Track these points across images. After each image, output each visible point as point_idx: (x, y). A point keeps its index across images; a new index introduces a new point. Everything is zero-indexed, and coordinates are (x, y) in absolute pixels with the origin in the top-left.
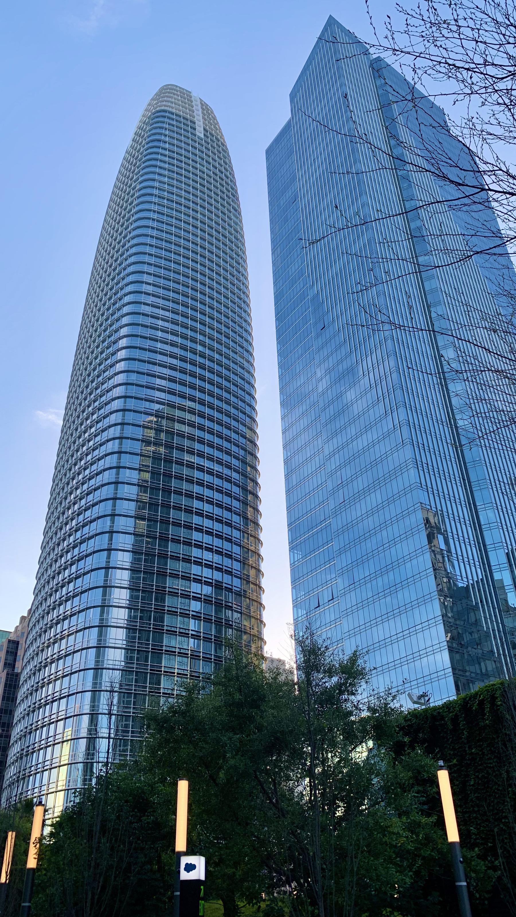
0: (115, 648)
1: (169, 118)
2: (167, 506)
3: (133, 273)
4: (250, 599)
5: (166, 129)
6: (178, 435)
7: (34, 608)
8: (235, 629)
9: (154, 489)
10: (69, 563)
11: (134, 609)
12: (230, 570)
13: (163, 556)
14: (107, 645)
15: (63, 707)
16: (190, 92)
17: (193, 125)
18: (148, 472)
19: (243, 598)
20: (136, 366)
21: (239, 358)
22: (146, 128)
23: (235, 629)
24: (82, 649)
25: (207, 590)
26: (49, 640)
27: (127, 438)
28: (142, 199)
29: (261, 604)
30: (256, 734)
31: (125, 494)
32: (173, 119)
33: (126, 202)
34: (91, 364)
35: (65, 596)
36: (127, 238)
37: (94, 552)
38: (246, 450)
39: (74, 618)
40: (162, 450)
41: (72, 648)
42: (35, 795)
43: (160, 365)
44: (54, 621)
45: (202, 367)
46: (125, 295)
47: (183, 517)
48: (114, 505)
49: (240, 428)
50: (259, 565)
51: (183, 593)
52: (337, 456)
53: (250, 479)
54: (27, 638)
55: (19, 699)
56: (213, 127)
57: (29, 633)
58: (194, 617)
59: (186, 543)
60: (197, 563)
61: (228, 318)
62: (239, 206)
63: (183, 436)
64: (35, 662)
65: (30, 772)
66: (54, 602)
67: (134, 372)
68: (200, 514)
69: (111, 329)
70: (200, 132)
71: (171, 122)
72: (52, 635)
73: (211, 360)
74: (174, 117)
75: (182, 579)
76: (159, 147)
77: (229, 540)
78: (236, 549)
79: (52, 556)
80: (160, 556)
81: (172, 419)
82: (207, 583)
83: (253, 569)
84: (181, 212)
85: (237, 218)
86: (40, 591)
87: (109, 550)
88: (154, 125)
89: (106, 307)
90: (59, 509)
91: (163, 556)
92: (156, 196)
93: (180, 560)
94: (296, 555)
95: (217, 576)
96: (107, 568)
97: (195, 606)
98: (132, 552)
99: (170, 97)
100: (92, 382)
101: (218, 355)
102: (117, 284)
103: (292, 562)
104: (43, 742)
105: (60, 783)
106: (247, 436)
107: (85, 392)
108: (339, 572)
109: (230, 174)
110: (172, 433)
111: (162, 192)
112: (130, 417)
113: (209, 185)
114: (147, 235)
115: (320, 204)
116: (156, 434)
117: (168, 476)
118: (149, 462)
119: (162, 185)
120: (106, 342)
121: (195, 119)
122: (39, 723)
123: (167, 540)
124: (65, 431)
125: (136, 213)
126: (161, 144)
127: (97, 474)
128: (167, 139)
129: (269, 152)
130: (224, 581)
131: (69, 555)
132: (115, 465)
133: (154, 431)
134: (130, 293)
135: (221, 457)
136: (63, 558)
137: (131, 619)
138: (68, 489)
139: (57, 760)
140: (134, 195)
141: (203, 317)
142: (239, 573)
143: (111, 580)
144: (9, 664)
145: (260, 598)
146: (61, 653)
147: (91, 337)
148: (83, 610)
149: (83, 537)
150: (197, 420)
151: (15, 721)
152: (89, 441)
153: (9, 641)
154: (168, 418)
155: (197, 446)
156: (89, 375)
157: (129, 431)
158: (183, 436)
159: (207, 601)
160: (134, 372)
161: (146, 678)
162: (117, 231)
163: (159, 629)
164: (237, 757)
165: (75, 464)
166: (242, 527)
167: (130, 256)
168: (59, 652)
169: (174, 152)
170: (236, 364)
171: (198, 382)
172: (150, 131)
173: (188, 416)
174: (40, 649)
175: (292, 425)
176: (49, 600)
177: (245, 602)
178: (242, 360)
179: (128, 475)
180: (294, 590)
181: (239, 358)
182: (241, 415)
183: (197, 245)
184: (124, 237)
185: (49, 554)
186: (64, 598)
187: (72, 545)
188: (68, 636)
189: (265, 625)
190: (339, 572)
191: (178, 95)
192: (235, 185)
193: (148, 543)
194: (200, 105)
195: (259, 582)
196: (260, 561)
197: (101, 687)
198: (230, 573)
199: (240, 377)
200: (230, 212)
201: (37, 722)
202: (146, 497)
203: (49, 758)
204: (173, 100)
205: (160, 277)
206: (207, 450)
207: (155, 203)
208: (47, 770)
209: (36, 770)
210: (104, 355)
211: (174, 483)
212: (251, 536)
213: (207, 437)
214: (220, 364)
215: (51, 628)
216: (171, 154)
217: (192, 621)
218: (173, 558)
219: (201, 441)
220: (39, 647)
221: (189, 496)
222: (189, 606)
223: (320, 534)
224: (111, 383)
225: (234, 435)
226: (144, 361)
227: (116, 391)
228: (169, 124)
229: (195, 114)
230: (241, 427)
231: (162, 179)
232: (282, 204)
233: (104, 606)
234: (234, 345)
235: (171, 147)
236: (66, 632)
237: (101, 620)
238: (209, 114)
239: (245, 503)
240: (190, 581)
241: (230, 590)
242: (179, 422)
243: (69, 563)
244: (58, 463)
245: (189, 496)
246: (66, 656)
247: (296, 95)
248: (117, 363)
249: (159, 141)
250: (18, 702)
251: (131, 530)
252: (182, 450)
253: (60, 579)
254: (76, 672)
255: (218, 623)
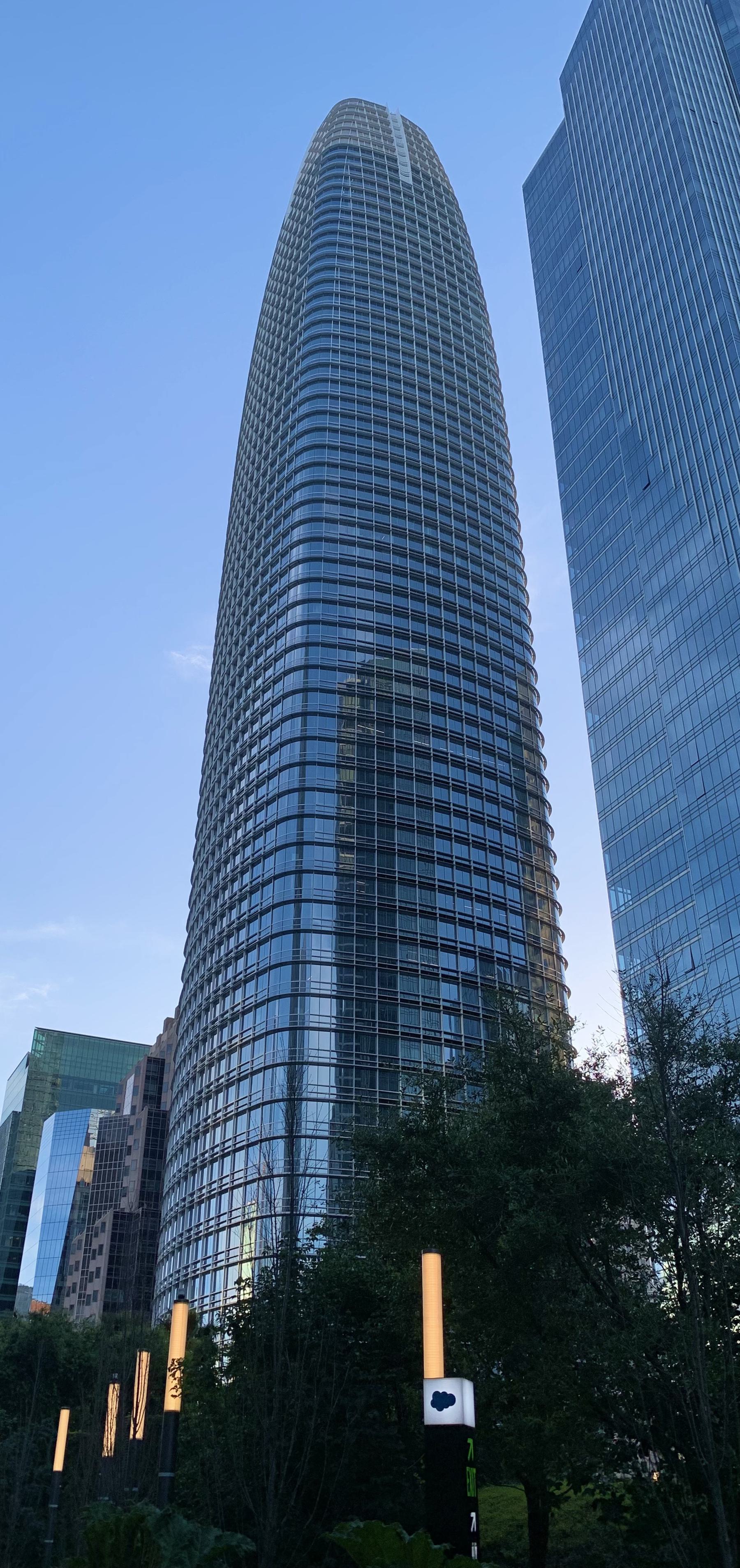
0: (318, 1064)
1: (351, 158)
2: (387, 825)
3: (306, 449)
4: (542, 978)
5: (346, 178)
6: (399, 702)
7: (184, 1003)
8: (516, 969)
9: (365, 797)
10: (235, 925)
11: (346, 999)
12: (505, 929)
13: (388, 910)
14: (306, 1025)
15: (240, 1164)
16: (384, 108)
17: (392, 165)
18: (352, 768)
19: (530, 977)
20: (322, 590)
21: (496, 562)
22: (313, 181)
23: (516, 969)
24: (265, 1068)
25: (467, 965)
26: (211, 1054)
27: (314, 738)
28: (314, 303)
29: (563, 986)
30: (564, 1167)
31: (317, 835)
32: (358, 159)
33: (290, 299)
34: (247, 594)
35: (230, 1012)
36: (293, 389)
37: (274, 906)
38: (518, 721)
39: (249, 1017)
40: (374, 730)
41: (249, 1066)
42: (205, 1308)
43: (361, 606)
44: (217, 1023)
45: (433, 582)
46: (296, 472)
47: (416, 841)
48: (300, 827)
49: (506, 683)
50: (555, 920)
51: (427, 969)
52: (686, 713)
53: (530, 771)
54: (176, 1052)
55: (170, 1153)
56: (427, 163)
57: (178, 1045)
58: (448, 1010)
59: (427, 975)
60: (446, 919)
61: (476, 510)
62: (482, 296)
63: (407, 704)
64: (191, 1092)
65: (194, 1272)
66: (215, 992)
67: (317, 601)
68: (444, 809)
69: (277, 531)
70: (406, 176)
71: (355, 164)
72: (215, 1046)
73: (449, 568)
74: (360, 154)
75: (423, 977)
76: (337, 211)
77: (500, 879)
78: (513, 894)
79: (204, 943)
80: (381, 823)
81: (385, 675)
82: (466, 953)
83: (544, 927)
84: (382, 318)
85: (480, 317)
86: (192, 974)
87: (297, 932)
88: (327, 174)
89: (265, 513)
90: (213, 839)
91: (388, 910)
92: (337, 295)
93: (416, 915)
94: (620, 895)
95: (483, 940)
96: (297, 932)
97: (449, 992)
98: (336, 903)
99: (350, 121)
100: (252, 624)
101: (459, 559)
102: (280, 472)
103: (615, 907)
104: (212, 1223)
105: (247, 1249)
106: (520, 696)
107: (240, 643)
108: (697, 886)
109: (463, 241)
110: (389, 700)
111: (346, 288)
112: (317, 678)
113: (427, 266)
114: (326, 365)
115: (627, 265)
116: (362, 705)
117: (386, 773)
118: (352, 752)
119: (346, 275)
120: (270, 555)
121: (396, 154)
122: (204, 1191)
123: (391, 881)
124: (213, 710)
125: (306, 328)
126: (341, 205)
127: (270, 777)
128: (350, 195)
129: (528, 188)
130: (495, 949)
131: (234, 914)
132: (296, 785)
133: (357, 700)
134: (304, 467)
135: (476, 736)
136: (227, 892)
137: (342, 1018)
138: (222, 830)
139: (237, 1252)
140: (299, 298)
141: (430, 496)
142: (521, 934)
143: (304, 952)
144: (152, 1098)
145: (561, 976)
146: (231, 1075)
147: (245, 549)
148: (262, 1004)
149: (253, 911)
150: (430, 674)
151: (166, 1190)
152: (251, 746)
153: (150, 1060)
154: (380, 675)
155: (432, 720)
156: (244, 634)
157: (317, 701)
158: (407, 704)
159: (467, 982)
160: (317, 601)
161: (374, 1041)
162: (275, 365)
163: (390, 999)
164: (531, 1211)
165: (234, 764)
166: (515, 803)
167: (300, 420)
168: (228, 1074)
169: (362, 216)
170: (494, 590)
171: (427, 609)
172: (319, 184)
173: (413, 669)
174: (198, 1069)
175: (600, 665)
176: (204, 1018)
177: (534, 984)
178: (502, 565)
179: (317, 802)
180: (607, 856)
181: (496, 562)
182: (506, 661)
183: (411, 342)
184: (288, 389)
185: (202, 913)
186: (230, 984)
187: (237, 897)
188: (241, 1046)
189: (566, 964)
190: (697, 886)
191: (363, 116)
192: (473, 259)
193: (360, 887)
194: (402, 128)
195: (558, 948)
196: (557, 912)
197: (304, 1023)
198: (504, 934)
199: (501, 595)
200: (467, 308)
201: (200, 1190)
202: (353, 811)
203: (226, 1210)
204: (356, 126)
205: (353, 469)
206: (450, 725)
207: (336, 308)
208: (221, 1268)
209: (204, 1268)
210: (266, 597)
211: (398, 865)
212: (538, 869)
213: (449, 702)
214: (464, 594)
215: (213, 1034)
216: (359, 220)
217: (444, 1018)
218: (404, 911)
219: (439, 711)
220: (195, 1066)
221: (424, 779)
222: (437, 959)
223: (663, 856)
224: (281, 644)
225: (491, 654)
226: (334, 582)
227: (291, 636)
228: (352, 168)
229: (395, 144)
230: (507, 682)
231: (346, 264)
232: (558, 277)
233: (296, 995)
234: (488, 539)
235: (358, 208)
236: (237, 1040)
237: (293, 1018)
238: (420, 142)
239: (523, 813)
240: (437, 949)
241: (507, 964)
242: (399, 680)
243: (235, 925)
244: (207, 743)
245: (424, 779)
246: (240, 1080)
247: (572, 76)
248: (288, 610)
249: (337, 199)
250: (168, 1158)
251: (332, 867)
252: (408, 728)
253: (222, 954)
254: (257, 1106)
255: (488, 988)
